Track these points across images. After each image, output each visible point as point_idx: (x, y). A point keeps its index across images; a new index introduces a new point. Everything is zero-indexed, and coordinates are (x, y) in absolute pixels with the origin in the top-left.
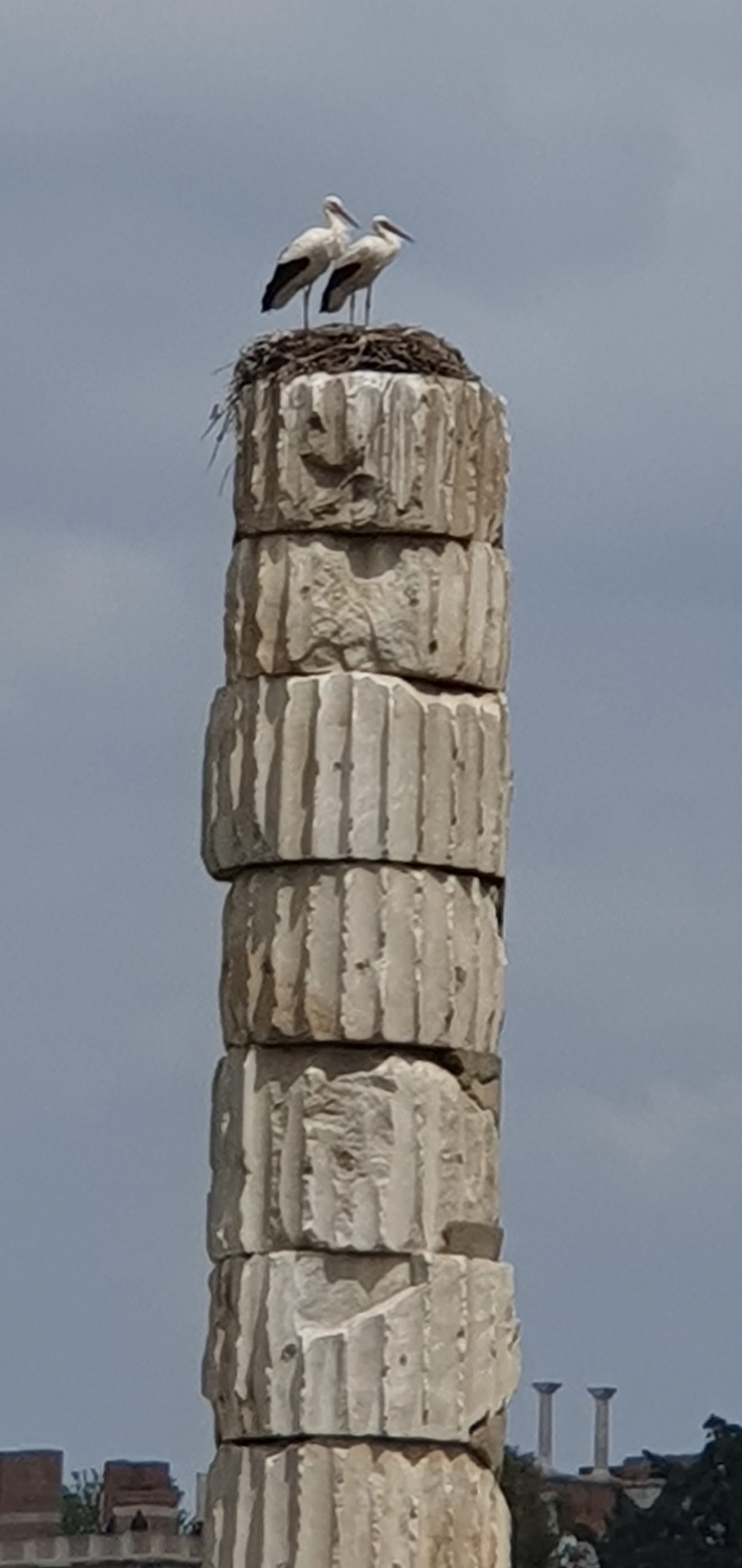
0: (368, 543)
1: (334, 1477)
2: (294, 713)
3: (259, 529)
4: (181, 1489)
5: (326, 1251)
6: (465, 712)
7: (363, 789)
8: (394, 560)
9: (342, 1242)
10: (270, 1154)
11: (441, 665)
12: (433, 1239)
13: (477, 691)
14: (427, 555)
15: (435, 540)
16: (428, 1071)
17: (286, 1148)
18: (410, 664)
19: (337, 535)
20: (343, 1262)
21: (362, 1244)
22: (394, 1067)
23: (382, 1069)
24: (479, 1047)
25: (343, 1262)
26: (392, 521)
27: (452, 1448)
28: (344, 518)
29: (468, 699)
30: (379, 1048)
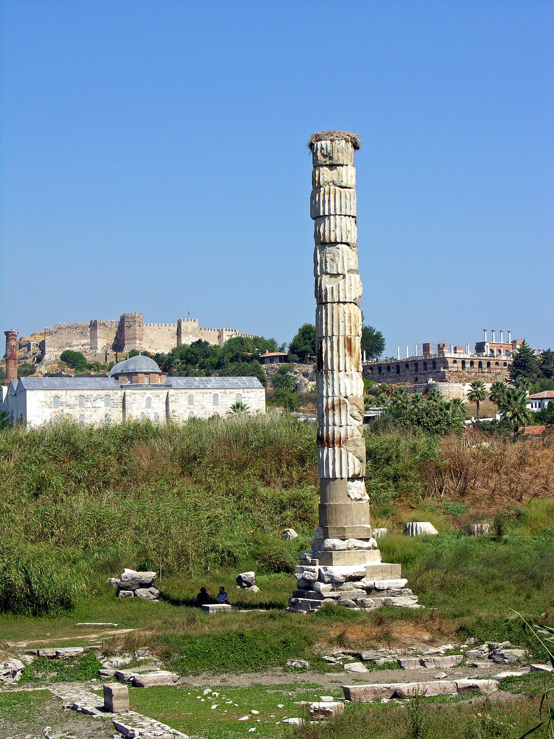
0: (332, 166)
1: (333, 308)
2: (322, 193)
3: (317, 165)
4: (475, 345)
8: (336, 168)
9: (332, 273)
10: (321, 260)
11: (343, 184)
12: (346, 272)
13: (350, 188)
14: (341, 167)
15: (342, 165)
16: (346, 246)
17: (324, 259)
18: (339, 185)
19: (327, 166)
20: (332, 275)
21: (335, 273)
22: (339, 246)
23: (337, 246)
25: (332, 275)
26: (335, 163)
28: (328, 163)
29: (348, 189)
30: (336, 243)
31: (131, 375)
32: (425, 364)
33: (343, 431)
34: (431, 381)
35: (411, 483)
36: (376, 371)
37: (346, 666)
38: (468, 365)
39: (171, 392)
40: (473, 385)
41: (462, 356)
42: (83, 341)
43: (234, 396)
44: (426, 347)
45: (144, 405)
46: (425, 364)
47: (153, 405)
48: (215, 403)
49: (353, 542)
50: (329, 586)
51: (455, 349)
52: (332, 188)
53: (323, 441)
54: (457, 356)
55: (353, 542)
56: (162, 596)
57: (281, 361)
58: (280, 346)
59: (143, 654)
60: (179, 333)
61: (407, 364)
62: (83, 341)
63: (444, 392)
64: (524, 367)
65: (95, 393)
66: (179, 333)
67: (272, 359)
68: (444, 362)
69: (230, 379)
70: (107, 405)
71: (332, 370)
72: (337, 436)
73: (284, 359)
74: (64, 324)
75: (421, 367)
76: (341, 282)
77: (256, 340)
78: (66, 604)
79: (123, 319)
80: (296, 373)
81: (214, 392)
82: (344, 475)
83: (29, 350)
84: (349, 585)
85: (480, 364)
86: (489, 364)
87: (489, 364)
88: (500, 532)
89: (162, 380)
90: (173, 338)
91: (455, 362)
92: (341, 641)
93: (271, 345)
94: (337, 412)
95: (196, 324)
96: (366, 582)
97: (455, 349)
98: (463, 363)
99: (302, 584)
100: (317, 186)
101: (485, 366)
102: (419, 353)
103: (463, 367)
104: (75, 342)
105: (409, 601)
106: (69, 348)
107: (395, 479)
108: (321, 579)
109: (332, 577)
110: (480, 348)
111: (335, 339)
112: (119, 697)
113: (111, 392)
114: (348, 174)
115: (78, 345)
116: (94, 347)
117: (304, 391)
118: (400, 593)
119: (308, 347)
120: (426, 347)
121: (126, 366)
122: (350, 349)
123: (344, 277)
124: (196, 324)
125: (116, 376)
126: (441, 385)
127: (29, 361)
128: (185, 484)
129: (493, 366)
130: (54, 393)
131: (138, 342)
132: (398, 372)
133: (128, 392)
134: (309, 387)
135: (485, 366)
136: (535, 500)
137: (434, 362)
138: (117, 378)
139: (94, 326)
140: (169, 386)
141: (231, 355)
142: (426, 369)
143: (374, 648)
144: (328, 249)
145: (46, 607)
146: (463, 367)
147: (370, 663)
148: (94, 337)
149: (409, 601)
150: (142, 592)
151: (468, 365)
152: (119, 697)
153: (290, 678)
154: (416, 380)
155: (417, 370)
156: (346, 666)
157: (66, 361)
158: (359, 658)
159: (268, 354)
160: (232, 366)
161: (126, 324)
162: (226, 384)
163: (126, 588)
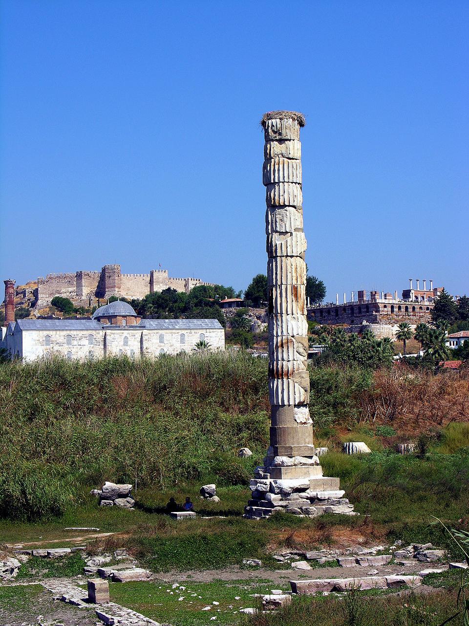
0: (281, 141)
3: (268, 140)
5: (279, 232)
6: (130, 313)
7: (281, 173)
10: (272, 220)
11: (291, 156)
13: (296, 159)
15: (290, 140)
16: (291, 208)
19: (276, 140)
20: (281, 233)
22: (287, 208)
23: (285, 209)
24: (299, 205)
25: (281, 233)
26: (284, 138)
27: (297, 256)
28: (278, 138)
30: (285, 206)
31: (111, 318)
33: (290, 365)
34: (365, 323)
36: (319, 315)
37: (293, 564)
39: (145, 332)
40: (401, 326)
43: (198, 335)
44: (361, 294)
45: (122, 343)
47: (129, 343)
50: (279, 497)
52: (281, 159)
54: (386, 301)
55: (299, 459)
58: (237, 293)
60: (151, 282)
62: (70, 289)
65: (80, 333)
66: (151, 282)
67: (230, 304)
68: (376, 307)
69: (195, 321)
71: (281, 313)
72: (285, 369)
74: (54, 275)
76: (289, 239)
77: (217, 288)
79: (104, 270)
80: (250, 316)
82: (292, 403)
83: (25, 296)
84: (295, 495)
85: (407, 308)
86: (414, 308)
88: (423, 451)
90: (146, 286)
93: (229, 292)
94: (285, 349)
95: (166, 275)
96: (310, 493)
97: (385, 295)
98: (392, 307)
100: (268, 158)
101: (410, 310)
102: (354, 299)
103: (392, 311)
104: (63, 290)
105: (346, 509)
108: (272, 490)
110: (406, 294)
111: (283, 287)
112: (101, 591)
113: (94, 332)
114: (295, 148)
115: (66, 292)
116: (79, 294)
117: (258, 331)
118: (339, 503)
119: (262, 294)
120: (361, 294)
121: (107, 310)
124: (166, 275)
125: (98, 319)
126: (373, 326)
129: (417, 310)
131: (117, 289)
132: (337, 315)
133: (108, 332)
134: (262, 328)
135: (410, 310)
137: (367, 306)
138: (99, 320)
139: (79, 276)
140: (143, 327)
141: (195, 301)
143: (316, 549)
144: (278, 211)
145: (39, 514)
146: (392, 311)
148: (79, 286)
149: (346, 509)
150: (120, 501)
151: (396, 310)
152: (101, 591)
153: (246, 574)
155: (352, 313)
157: (56, 305)
158: (304, 557)
159: (227, 300)
160: (196, 310)
161: (107, 274)
162: (192, 326)
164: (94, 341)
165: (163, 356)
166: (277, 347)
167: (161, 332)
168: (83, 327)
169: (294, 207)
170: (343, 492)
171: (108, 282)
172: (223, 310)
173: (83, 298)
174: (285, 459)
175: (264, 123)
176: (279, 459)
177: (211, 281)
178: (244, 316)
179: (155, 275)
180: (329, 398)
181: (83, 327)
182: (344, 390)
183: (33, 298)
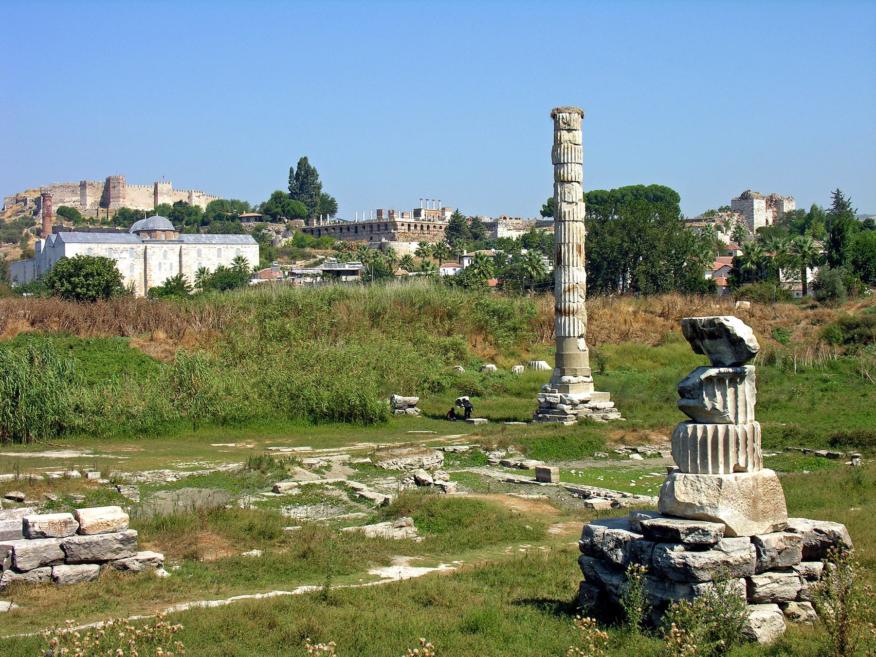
0: (569, 130)
3: (557, 129)
20: (569, 203)
25: (569, 203)
31: (150, 232)
32: (379, 226)
33: (575, 305)
34: (384, 240)
35: (524, 333)
36: (338, 231)
37: (631, 456)
38: (412, 228)
39: (184, 246)
40: (420, 244)
41: (408, 220)
42: (74, 199)
43: (234, 250)
44: (379, 213)
45: (162, 256)
46: (379, 226)
47: (168, 257)
48: (219, 256)
49: (581, 378)
50: (570, 407)
51: (403, 214)
52: (570, 145)
53: (559, 312)
54: (404, 220)
55: (581, 378)
56: (425, 414)
57: (256, 220)
58: (252, 207)
59: (511, 449)
60: (156, 193)
61: (364, 226)
62: (74, 199)
63: (396, 249)
64: (457, 231)
65: (122, 246)
66: (156, 193)
67: (248, 219)
68: (394, 225)
69: (230, 236)
70: (131, 256)
71: (569, 266)
72: (571, 309)
73: (259, 219)
74: (58, 184)
75: (375, 228)
76: (575, 207)
77: (233, 203)
78: (383, 419)
79: (108, 180)
80: (269, 230)
81: (218, 246)
82: (576, 335)
83: (26, 204)
84: (581, 406)
85: (422, 226)
86: (428, 227)
87: (428, 227)
88: (602, 369)
89: (176, 236)
90: (151, 197)
91: (403, 225)
92: (622, 440)
93: (244, 207)
94: (571, 293)
95: (170, 186)
96: (592, 404)
97: (403, 214)
98: (409, 226)
99: (545, 405)
100: (557, 143)
101: (425, 228)
102: (373, 217)
103: (409, 229)
104: (67, 199)
105: (615, 415)
106: (61, 204)
107: (515, 329)
108: (562, 401)
109: (572, 401)
110: (417, 213)
111: (571, 245)
112: (554, 474)
113: (134, 246)
114: (578, 136)
115: (70, 201)
116: (83, 204)
117: (279, 246)
118: (611, 411)
119: (279, 210)
120: (379, 213)
121: (146, 224)
122: (580, 252)
123: (577, 204)
124: (170, 186)
125: (138, 233)
126: (393, 244)
127: (27, 214)
128: (375, 333)
129: (431, 228)
130: (88, 246)
131: (122, 200)
132: (356, 232)
133: (149, 246)
134: (283, 243)
135: (425, 228)
136: (605, 345)
137: (386, 225)
138: (138, 234)
139: (83, 185)
140: (182, 242)
141: (213, 214)
142: (379, 230)
143: (643, 445)
144: (566, 185)
145: (371, 421)
146: (409, 229)
147: (643, 454)
148: (83, 195)
149: (615, 415)
150: (409, 410)
151: (412, 228)
152: (554, 474)
153: (599, 464)
154: (371, 238)
155: (372, 231)
156: (631, 456)
157: (62, 215)
158: (635, 451)
159: (245, 215)
160: (218, 224)
161: (112, 185)
162: (227, 241)
163: (400, 408)
164: (134, 254)
165: (221, 269)
166: (565, 292)
167: (198, 246)
168: (123, 240)
169: (578, 182)
170: (612, 404)
171: (112, 192)
172: (243, 224)
173: (87, 207)
174: (571, 378)
175: (554, 116)
176: (565, 378)
177: (228, 197)
178: (264, 231)
179: (160, 186)
180: (508, 323)
181: (123, 240)
182: (519, 317)
183: (35, 207)
